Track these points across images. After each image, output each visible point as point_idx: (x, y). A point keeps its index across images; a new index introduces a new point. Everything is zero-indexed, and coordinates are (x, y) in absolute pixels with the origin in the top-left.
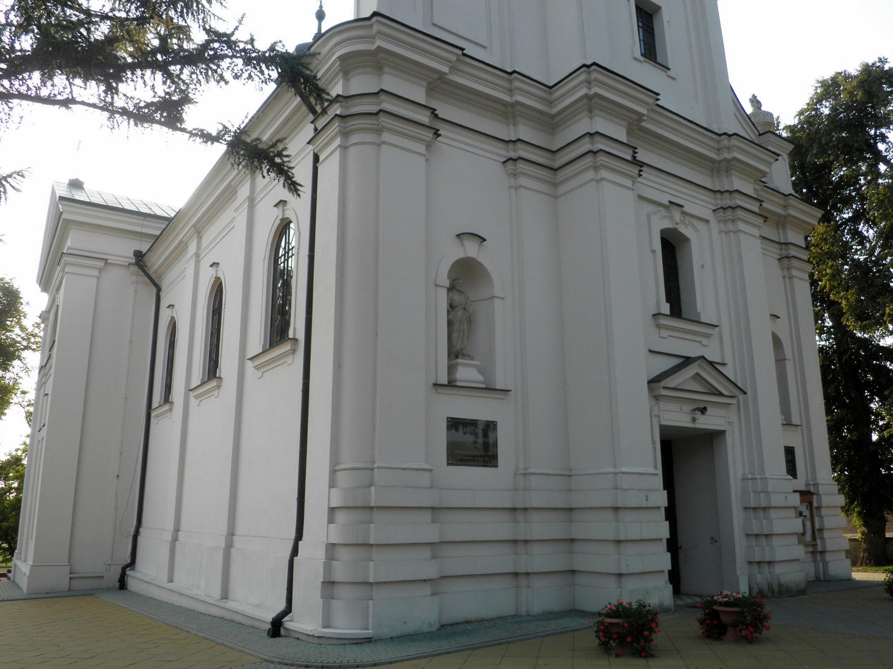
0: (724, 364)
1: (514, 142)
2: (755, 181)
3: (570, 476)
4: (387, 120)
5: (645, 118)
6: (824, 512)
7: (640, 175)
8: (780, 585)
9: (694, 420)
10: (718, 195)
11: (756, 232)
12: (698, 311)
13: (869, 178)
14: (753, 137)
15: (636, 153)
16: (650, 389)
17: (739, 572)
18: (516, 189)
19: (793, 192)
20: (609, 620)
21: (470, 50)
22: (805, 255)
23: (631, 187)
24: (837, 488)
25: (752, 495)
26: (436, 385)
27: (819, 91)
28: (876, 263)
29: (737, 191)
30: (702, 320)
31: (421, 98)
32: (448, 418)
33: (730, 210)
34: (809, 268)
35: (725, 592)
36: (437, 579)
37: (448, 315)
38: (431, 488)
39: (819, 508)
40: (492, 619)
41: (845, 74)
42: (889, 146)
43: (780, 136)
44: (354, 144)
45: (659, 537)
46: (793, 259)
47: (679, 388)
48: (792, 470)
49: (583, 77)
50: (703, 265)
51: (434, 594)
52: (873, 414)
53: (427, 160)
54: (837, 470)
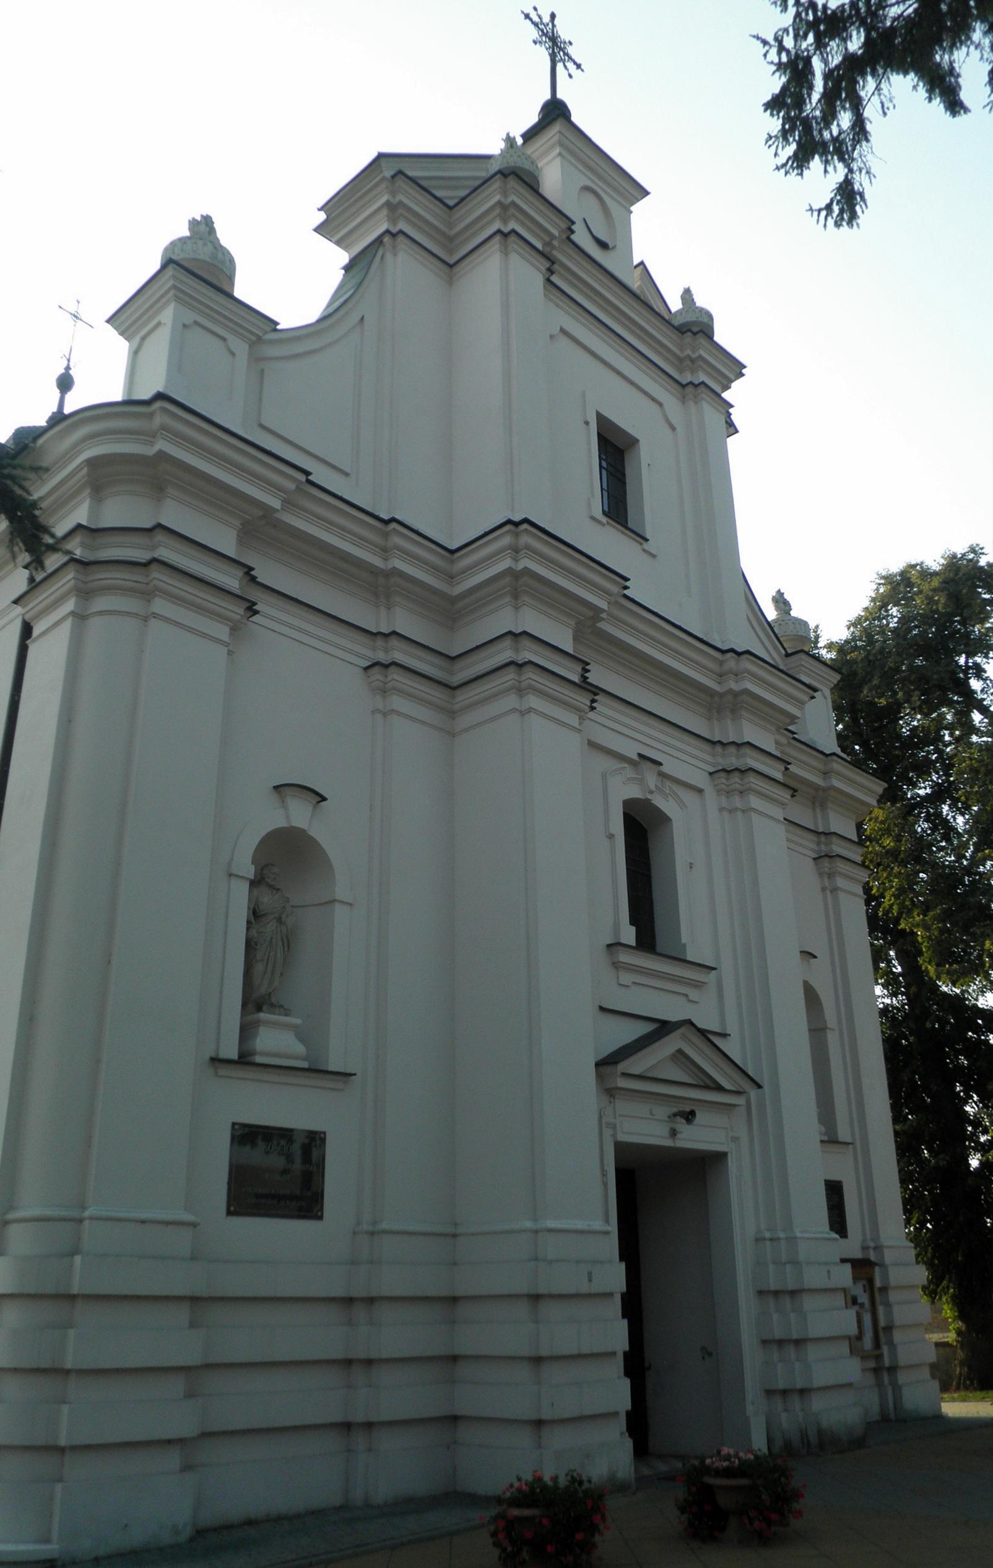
0: (724, 1035)
1: (386, 636)
2: (778, 729)
3: (454, 1236)
4: (164, 578)
5: (604, 615)
6: (893, 1296)
7: (593, 708)
8: (820, 1432)
9: (674, 1133)
10: (719, 749)
11: (778, 813)
12: (683, 941)
13: (957, 733)
14: (777, 658)
15: (588, 671)
16: (600, 1077)
17: (750, 1409)
18: (385, 715)
19: (838, 751)
20: (516, 1512)
21: (321, 475)
22: (856, 854)
23: (578, 727)
24: (913, 1253)
25: (771, 1267)
26: (216, 1061)
27: (882, 590)
28: (968, 871)
29: (748, 743)
30: (689, 958)
31: (227, 543)
32: (234, 1124)
33: (737, 774)
34: (863, 875)
35: (725, 1451)
36: (194, 1439)
37: (248, 929)
38: (193, 1258)
39: (884, 1289)
40: (298, 1516)
41: (922, 567)
42: (987, 685)
43: (818, 659)
44: (101, 613)
45: (610, 1350)
46: (838, 859)
47: (650, 1075)
48: (838, 1223)
49: (506, 540)
50: (691, 864)
51: (187, 1468)
52: (971, 1123)
53: (230, 653)
54: (913, 1221)
